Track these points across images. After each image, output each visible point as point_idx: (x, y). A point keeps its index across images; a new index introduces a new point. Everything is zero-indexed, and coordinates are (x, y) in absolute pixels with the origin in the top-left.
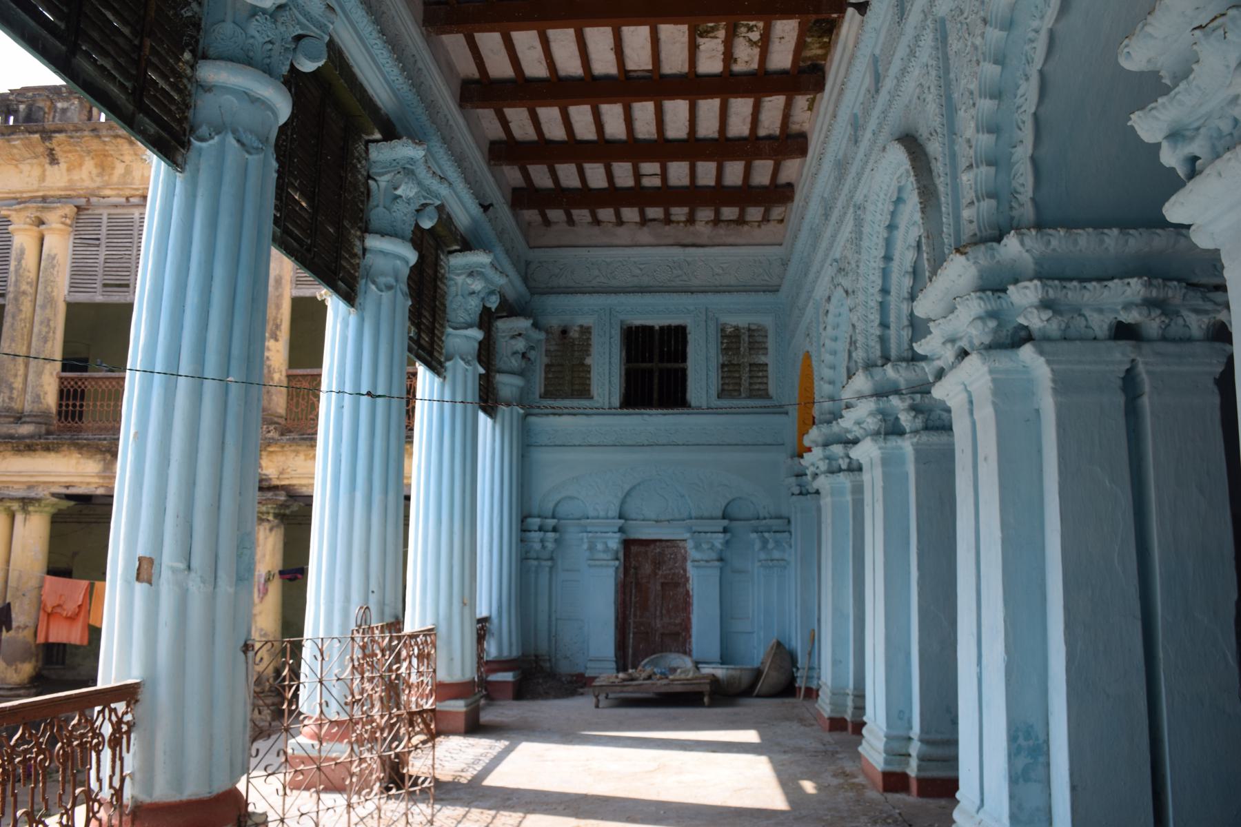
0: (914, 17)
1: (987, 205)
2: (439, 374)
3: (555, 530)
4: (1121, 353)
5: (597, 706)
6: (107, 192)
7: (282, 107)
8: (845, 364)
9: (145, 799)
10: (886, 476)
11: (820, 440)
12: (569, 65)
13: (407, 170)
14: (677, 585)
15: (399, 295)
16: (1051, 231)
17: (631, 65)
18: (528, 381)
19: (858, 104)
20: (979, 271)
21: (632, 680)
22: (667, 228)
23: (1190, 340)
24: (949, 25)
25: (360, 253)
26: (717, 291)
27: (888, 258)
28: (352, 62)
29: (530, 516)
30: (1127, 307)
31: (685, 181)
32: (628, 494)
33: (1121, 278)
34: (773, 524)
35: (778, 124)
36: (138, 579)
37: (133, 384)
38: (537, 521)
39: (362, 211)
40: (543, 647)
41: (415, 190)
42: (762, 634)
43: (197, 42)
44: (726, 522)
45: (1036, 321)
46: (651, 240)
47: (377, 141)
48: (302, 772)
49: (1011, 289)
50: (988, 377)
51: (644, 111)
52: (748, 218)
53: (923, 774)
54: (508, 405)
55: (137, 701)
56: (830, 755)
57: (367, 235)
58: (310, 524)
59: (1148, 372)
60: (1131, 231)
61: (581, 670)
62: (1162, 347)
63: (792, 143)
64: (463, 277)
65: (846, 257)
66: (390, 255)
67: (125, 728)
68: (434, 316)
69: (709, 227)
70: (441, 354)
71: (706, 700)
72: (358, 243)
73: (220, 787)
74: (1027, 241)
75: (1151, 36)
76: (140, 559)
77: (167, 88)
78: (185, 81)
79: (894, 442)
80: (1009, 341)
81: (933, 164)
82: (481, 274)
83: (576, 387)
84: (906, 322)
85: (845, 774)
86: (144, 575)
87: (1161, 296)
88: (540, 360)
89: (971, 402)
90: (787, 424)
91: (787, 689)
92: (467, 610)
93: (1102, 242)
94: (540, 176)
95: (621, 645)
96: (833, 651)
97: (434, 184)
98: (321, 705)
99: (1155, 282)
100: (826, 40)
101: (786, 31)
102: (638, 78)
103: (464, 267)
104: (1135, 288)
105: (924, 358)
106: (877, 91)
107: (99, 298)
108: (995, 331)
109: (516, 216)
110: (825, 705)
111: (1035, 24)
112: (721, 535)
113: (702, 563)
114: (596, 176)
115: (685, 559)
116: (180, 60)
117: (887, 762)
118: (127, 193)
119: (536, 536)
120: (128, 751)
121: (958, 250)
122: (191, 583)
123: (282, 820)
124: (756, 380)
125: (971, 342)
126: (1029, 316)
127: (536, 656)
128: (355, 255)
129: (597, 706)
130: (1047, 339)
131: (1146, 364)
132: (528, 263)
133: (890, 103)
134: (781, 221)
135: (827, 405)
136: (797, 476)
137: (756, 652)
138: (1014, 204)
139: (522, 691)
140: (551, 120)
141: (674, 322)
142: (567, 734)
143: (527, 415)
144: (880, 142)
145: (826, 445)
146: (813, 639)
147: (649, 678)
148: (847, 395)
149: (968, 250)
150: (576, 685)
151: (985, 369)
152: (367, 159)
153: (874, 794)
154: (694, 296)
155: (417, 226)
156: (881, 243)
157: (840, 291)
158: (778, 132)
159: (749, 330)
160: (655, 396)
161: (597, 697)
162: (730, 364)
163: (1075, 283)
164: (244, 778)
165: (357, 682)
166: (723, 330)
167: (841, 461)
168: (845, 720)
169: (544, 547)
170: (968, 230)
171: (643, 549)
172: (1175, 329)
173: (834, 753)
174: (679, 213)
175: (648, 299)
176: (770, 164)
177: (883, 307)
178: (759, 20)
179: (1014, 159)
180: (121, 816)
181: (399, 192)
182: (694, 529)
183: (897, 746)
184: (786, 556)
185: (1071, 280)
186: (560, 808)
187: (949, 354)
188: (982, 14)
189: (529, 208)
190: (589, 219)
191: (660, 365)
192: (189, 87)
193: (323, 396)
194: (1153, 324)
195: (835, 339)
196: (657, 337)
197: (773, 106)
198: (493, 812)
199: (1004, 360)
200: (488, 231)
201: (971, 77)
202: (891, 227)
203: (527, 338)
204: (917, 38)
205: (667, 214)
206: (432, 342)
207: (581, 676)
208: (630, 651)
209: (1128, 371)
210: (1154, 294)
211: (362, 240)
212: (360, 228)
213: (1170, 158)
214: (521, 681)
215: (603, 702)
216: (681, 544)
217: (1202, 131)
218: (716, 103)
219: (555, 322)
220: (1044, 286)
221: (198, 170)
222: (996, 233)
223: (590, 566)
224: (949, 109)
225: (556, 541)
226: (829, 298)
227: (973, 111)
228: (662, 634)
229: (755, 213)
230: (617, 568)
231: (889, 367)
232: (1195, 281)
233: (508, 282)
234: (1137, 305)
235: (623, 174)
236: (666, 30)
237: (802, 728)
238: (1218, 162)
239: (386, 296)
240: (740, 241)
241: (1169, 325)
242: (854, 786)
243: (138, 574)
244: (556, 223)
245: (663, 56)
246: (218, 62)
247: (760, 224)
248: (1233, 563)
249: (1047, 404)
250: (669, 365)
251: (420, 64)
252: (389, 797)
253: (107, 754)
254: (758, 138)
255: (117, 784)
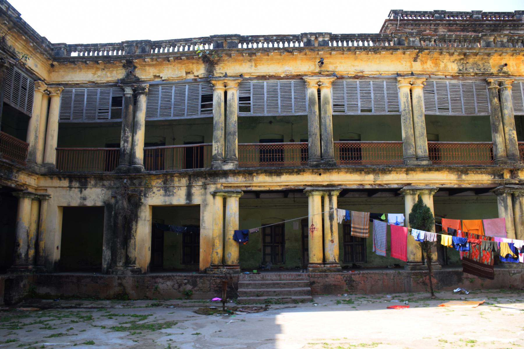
6: (439, 73)
107: (438, 113)
118: (447, 74)
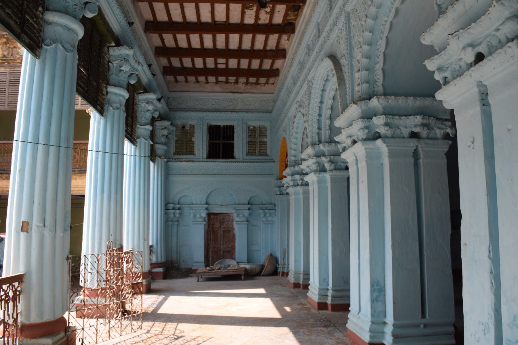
0: (336, 10)
1: (365, 86)
2: (134, 144)
3: (179, 209)
4: (413, 143)
5: (198, 281)
7: (80, 32)
8: (300, 143)
9: (27, 322)
10: (319, 188)
11: (290, 173)
12: (191, 17)
13: (125, 59)
14: (229, 231)
15: (122, 111)
16: (389, 97)
17: (217, 19)
18: (168, 147)
19: (310, 41)
20: (362, 111)
21: (213, 270)
22: (227, 85)
23: (437, 139)
24: (351, 15)
25: (105, 93)
26: (246, 112)
27: (321, 102)
28: (104, 13)
29: (169, 203)
30: (415, 126)
31: (235, 66)
32: (209, 194)
33: (414, 115)
34: (269, 206)
35: (275, 45)
36: (22, 231)
37: (17, 148)
38: (172, 205)
39: (106, 76)
40: (175, 257)
41: (129, 68)
42: (264, 251)
43: (44, 3)
44: (250, 206)
45: (383, 130)
46: (220, 90)
47: (113, 47)
48: (90, 309)
49: (374, 118)
50: (364, 151)
51: (221, 38)
52: (260, 82)
53: (336, 303)
54: (160, 157)
55: (22, 282)
56: (295, 297)
57: (108, 86)
58: (84, 207)
59: (422, 150)
60: (418, 98)
61: (190, 267)
62: (427, 141)
63: (280, 53)
64: (144, 104)
65: (303, 101)
66: (118, 94)
67: (18, 293)
68: (132, 120)
69: (244, 85)
70: (135, 136)
71: (243, 277)
72: (105, 89)
73: (58, 316)
74: (381, 101)
75: (432, 33)
76: (23, 222)
77: (33, 22)
78: (40, 20)
79: (323, 174)
80: (372, 137)
81: (343, 68)
82: (152, 103)
83: (188, 150)
84: (328, 128)
85: (302, 304)
86: (25, 229)
87: (427, 122)
88: (173, 138)
89: (357, 160)
90: (275, 167)
91: (275, 273)
92: (146, 242)
93: (407, 102)
94: (176, 62)
95: (207, 256)
96: (295, 257)
97: (136, 65)
98: (98, 281)
99: (425, 117)
100: (296, 13)
101: (281, 9)
102: (220, 24)
103: (145, 100)
104: (419, 119)
105: (338, 143)
106: (319, 36)
108: (368, 134)
109: (164, 78)
110: (291, 278)
111: (385, 19)
112: (248, 211)
113: (240, 222)
114: (199, 63)
115: (233, 221)
116: (37, 10)
117: (319, 299)
119: (171, 211)
120: (19, 303)
121: (354, 103)
122: (45, 232)
123: (83, 329)
124: (262, 148)
125: (357, 138)
126: (381, 129)
127: (172, 261)
128: (103, 95)
129: (198, 281)
130: (386, 137)
131: (422, 147)
132: (168, 98)
133: (325, 42)
134: (273, 84)
135: (293, 158)
136: (279, 187)
137: (262, 258)
138: (375, 86)
139: (166, 276)
140: (182, 40)
141: (229, 124)
142: (187, 292)
143: (168, 161)
144: (320, 57)
145: (292, 175)
146: (286, 253)
147: (219, 269)
148: (304, 156)
149: (358, 102)
150: (188, 273)
151: (363, 148)
152: (108, 54)
153: (315, 311)
154: (238, 113)
155: (129, 83)
156: (319, 96)
157: (300, 114)
158: (274, 48)
159: (260, 128)
160: (221, 154)
161: (198, 277)
162: (252, 142)
163: (397, 117)
164: (67, 313)
165: (112, 271)
166: (249, 128)
167: (298, 182)
168: (300, 284)
169: (175, 216)
170: (357, 95)
171: (215, 217)
172: (432, 135)
173: (297, 297)
174: (232, 79)
175: (218, 114)
176: (270, 61)
177: (319, 121)
178: (270, 4)
179: (376, 69)
180: (17, 330)
181: (122, 69)
182: (237, 208)
183: (323, 292)
184: (274, 219)
185: (396, 115)
186: (192, 321)
187: (349, 142)
188: (365, 13)
189: (170, 75)
190: (195, 80)
191: (223, 141)
192: (41, 22)
193: (89, 153)
194: (424, 133)
195: (297, 133)
196: (222, 130)
197: (273, 38)
198: (164, 323)
199: (370, 145)
200: (154, 85)
201: (360, 37)
202: (323, 90)
203: (168, 129)
204: (337, 18)
205: (227, 79)
206: (132, 131)
207: (190, 269)
208: (211, 259)
209: (415, 150)
210: (425, 121)
211: (107, 88)
212: (105, 83)
213: (438, 77)
214: (168, 271)
215: (200, 280)
216: (231, 215)
217: (449, 68)
218: (250, 36)
219: (179, 123)
220: (386, 117)
221: (46, 58)
222: (368, 96)
223: (194, 224)
224: (350, 48)
225: (180, 214)
226: (295, 117)
227: (360, 49)
228: (223, 251)
229: (263, 80)
230: (205, 225)
231: (321, 145)
232: (439, 117)
233: (161, 106)
234: (419, 126)
235: (210, 63)
236: (232, 6)
237: (282, 288)
238: (455, 80)
239: (116, 112)
240: (256, 91)
241: (429, 133)
242: (306, 309)
243: (22, 229)
244: (180, 82)
245: (231, 16)
246: (54, 13)
247: (265, 84)
248: (450, 220)
249: (386, 162)
250: (227, 142)
251: (130, 14)
252: (125, 318)
253: (11, 304)
254: (266, 51)
255: (15, 317)
